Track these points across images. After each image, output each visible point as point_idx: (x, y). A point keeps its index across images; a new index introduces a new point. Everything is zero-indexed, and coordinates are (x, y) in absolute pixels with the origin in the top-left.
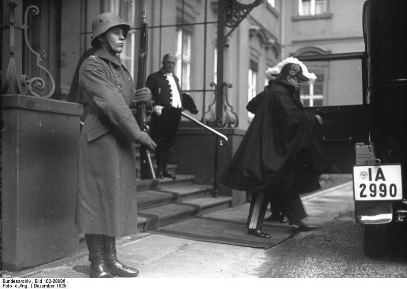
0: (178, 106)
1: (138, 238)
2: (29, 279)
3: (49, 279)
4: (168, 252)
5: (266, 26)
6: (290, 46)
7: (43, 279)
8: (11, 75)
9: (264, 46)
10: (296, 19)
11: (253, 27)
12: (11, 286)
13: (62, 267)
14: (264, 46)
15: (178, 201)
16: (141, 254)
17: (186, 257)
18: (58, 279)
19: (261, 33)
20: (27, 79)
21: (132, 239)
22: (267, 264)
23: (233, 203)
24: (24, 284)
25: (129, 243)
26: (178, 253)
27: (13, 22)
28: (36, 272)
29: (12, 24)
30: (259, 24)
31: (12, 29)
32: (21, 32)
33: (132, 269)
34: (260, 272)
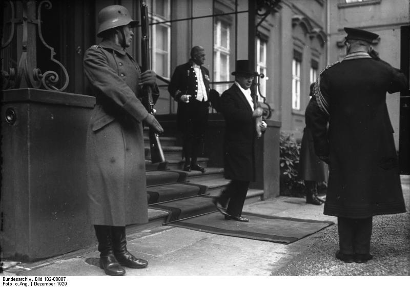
0: (203, 99)
1: (157, 232)
2: (30, 277)
3: (49, 277)
4: (185, 246)
5: (309, 15)
6: (336, 34)
7: (43, 277)
8: (23, 70)
11: (296, 16)
12: (11, 284)
13: (75, 259)
14: (308, 35)
16: (157, 247)
17: (201, 250)
18: (58, 277)
20: (39, 73)
21: (152, 232)
22: (284, 259)
23: (265, 197)
24: (25, 282)
25: (148, 236)
26: (194, 247)
27: (26, 17)
28: (48, 263)
29: (25, 19)
31: (25, 24)
33: (141, 260)
34: (275, 267)
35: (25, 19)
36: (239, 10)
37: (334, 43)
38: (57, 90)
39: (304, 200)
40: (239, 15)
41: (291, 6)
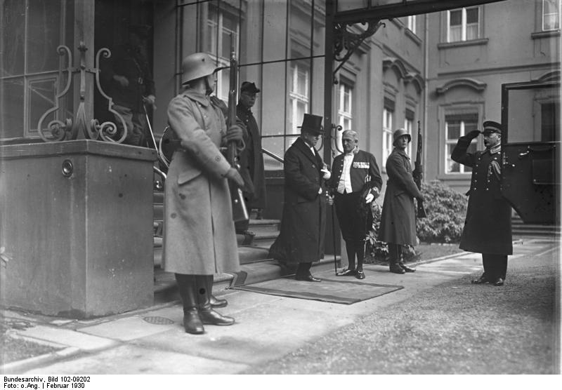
6: (435, 79)
9: (402, 80)
10: (442, 47)
11: (388, 59)
12: (15, 386)
15: (254, 244)
19: (396, 64)
20: (97, 124)
24: (34, 383)
29: (83, 68)
30: (395, 55)
31: (83, 72)
32: (92, 76)
35: (83, 68)
36: (314, 55)
37: (434, 89)
38: (113, 142)
39: (388, 268)
40: (309, 56)
41: (381, 46)
